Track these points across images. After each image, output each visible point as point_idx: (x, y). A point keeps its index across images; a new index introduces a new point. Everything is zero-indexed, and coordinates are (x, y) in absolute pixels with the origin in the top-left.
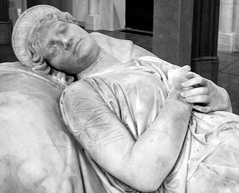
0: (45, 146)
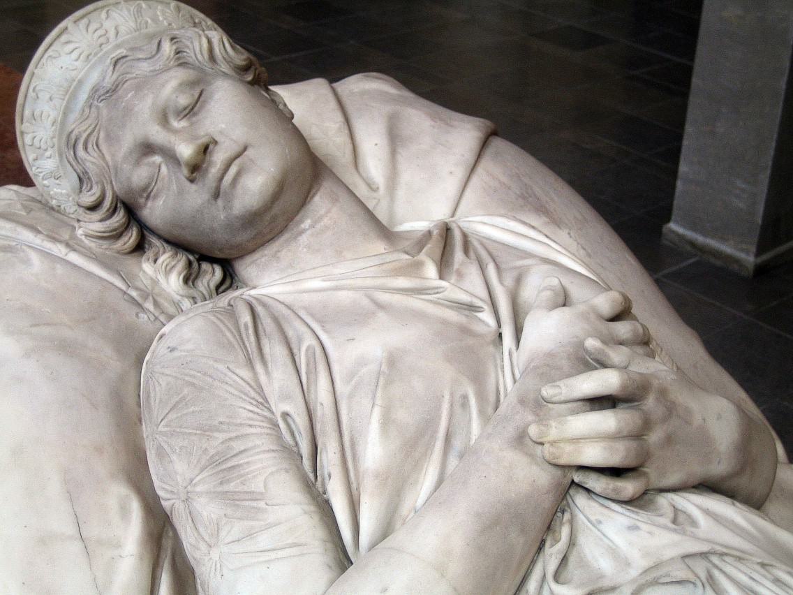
0: (45, 540)
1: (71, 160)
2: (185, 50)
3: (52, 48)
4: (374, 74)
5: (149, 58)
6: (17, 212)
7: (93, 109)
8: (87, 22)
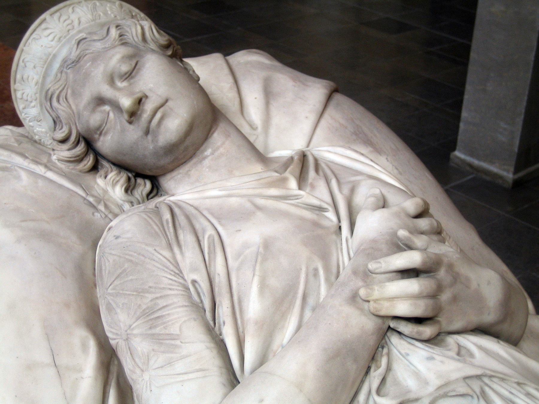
0: (30, 367)
2: (126, 34)
3: (36, 33)
5: (102, 40)
7: (63, 74)
8: (60, 15)
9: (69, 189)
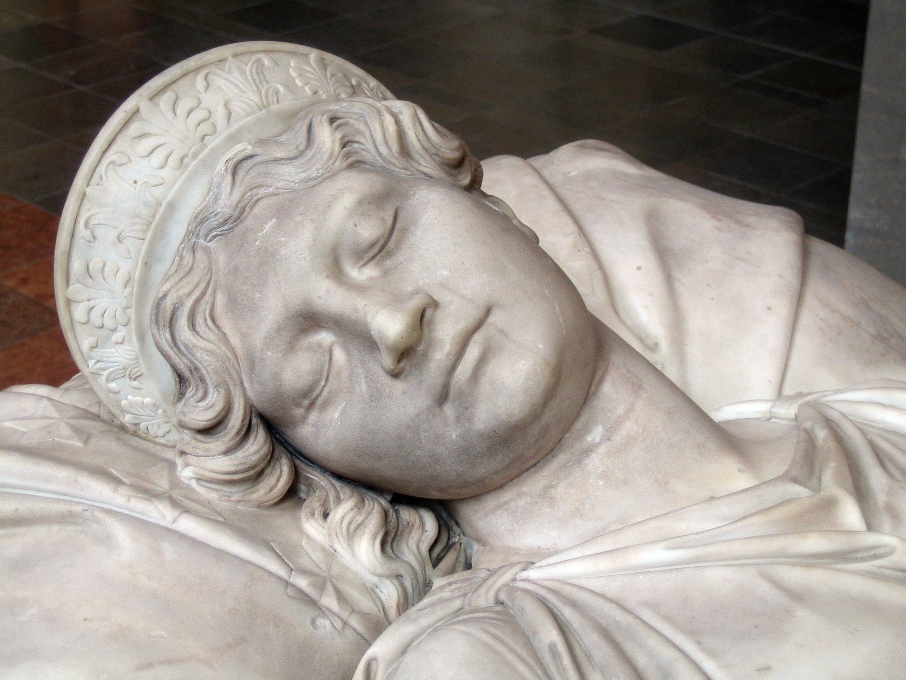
1: (167, 348)
2: (357, 139)
3: (114, 148)
4: (590, 142)
5: (295, 158)
6: (64, 441)
7: (200, 254)
8: (173, 97)
9: (245, 562)
